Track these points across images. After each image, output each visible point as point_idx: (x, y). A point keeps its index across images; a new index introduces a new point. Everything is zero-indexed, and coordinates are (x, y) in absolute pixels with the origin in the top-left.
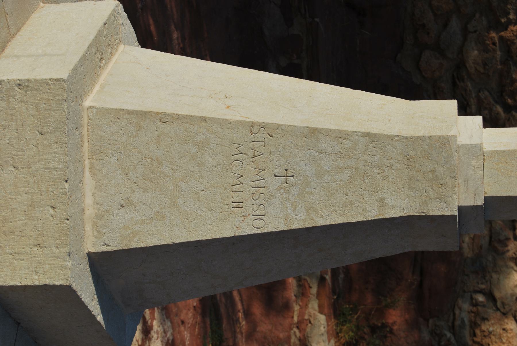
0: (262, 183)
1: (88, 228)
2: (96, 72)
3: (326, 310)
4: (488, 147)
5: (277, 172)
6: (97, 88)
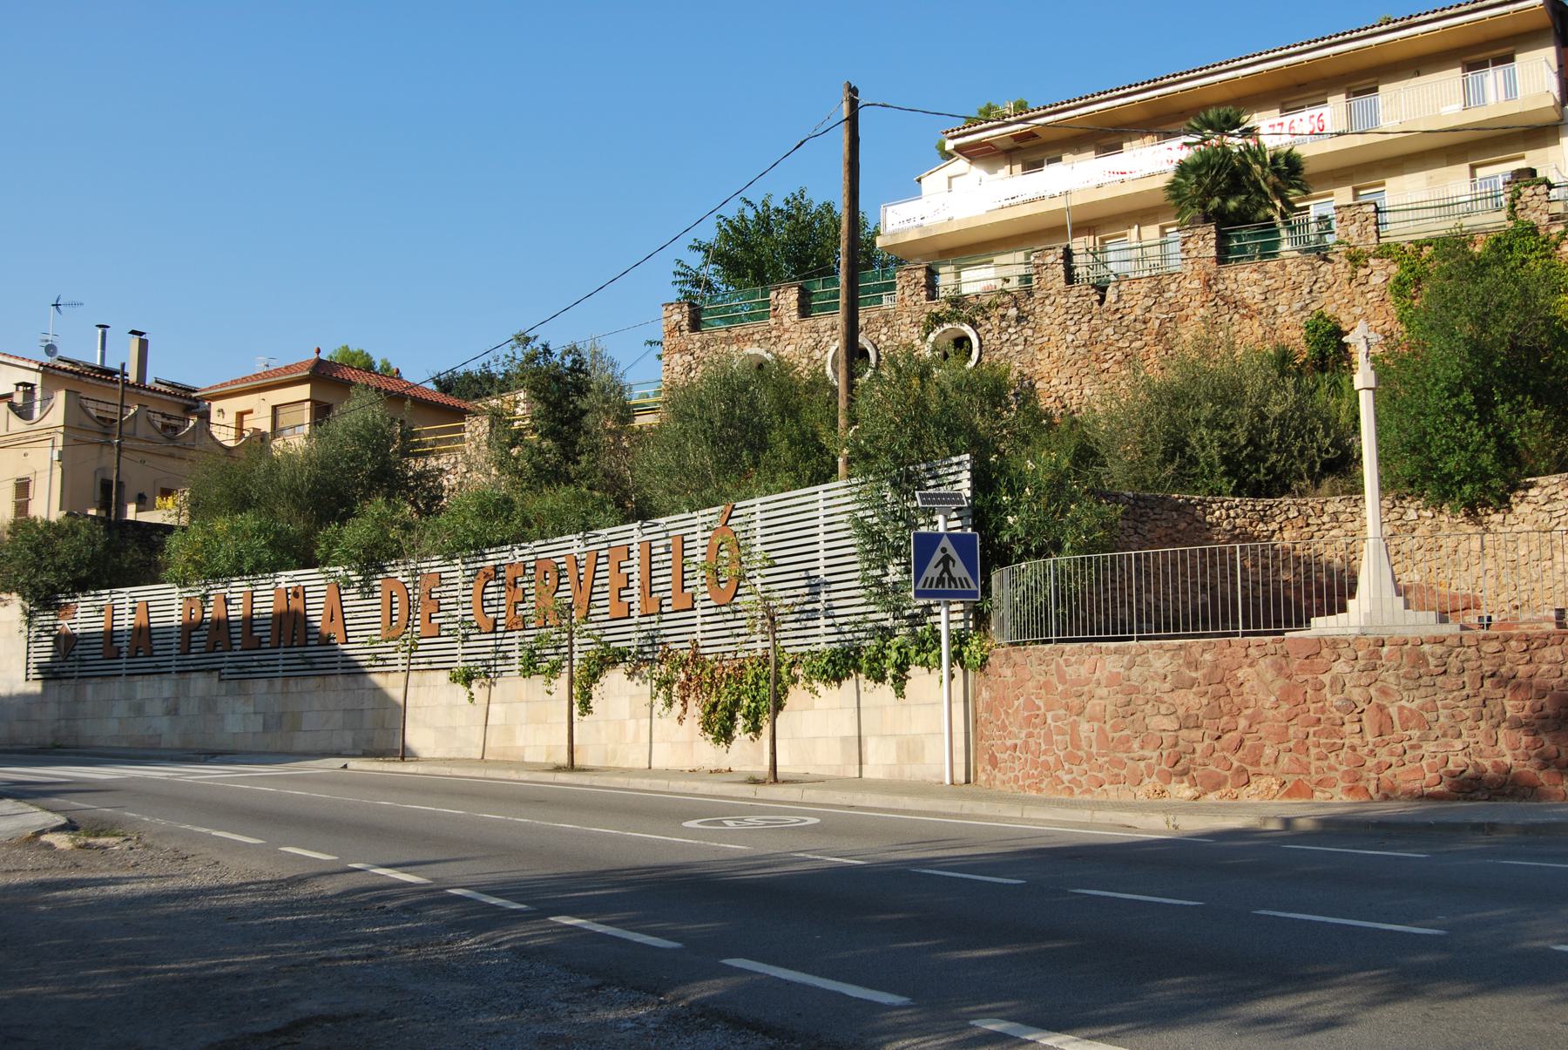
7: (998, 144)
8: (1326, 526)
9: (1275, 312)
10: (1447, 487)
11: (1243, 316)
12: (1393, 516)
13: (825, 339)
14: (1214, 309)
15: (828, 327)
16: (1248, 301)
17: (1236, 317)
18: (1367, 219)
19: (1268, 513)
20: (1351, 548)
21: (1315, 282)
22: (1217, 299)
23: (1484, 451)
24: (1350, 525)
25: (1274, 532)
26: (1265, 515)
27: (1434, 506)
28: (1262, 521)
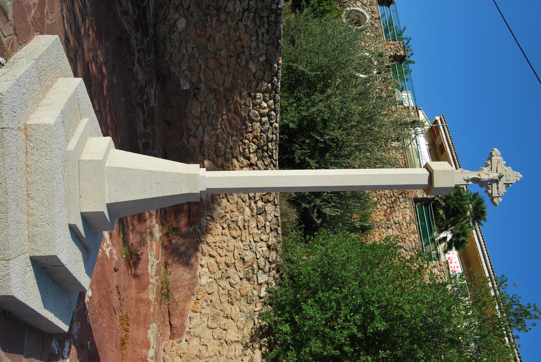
0: (151, 185)
1: (107, 197)
2: (107, 157)
3: (158, 223)
4: (207, 176)
5: (155, 182)
6: (108, 161)
7: (438, 139)
8: (253, 204)
9: (388, 228)
10: (288, 308)
11: (386, 211)
12: (262, 262)
13: (367, 8)
14: (389, 196)
15: (373, 10)
16: (394, 214)
17: (385, 207)
18: (441, 278)
19: (266, 154)
20: (233, 225)
21: (406, 250)
23: (324, 343)
24: (254, 224)
25: (249, 159)
26: (263, 151)
27: (270, 298)
28: (259, 148)
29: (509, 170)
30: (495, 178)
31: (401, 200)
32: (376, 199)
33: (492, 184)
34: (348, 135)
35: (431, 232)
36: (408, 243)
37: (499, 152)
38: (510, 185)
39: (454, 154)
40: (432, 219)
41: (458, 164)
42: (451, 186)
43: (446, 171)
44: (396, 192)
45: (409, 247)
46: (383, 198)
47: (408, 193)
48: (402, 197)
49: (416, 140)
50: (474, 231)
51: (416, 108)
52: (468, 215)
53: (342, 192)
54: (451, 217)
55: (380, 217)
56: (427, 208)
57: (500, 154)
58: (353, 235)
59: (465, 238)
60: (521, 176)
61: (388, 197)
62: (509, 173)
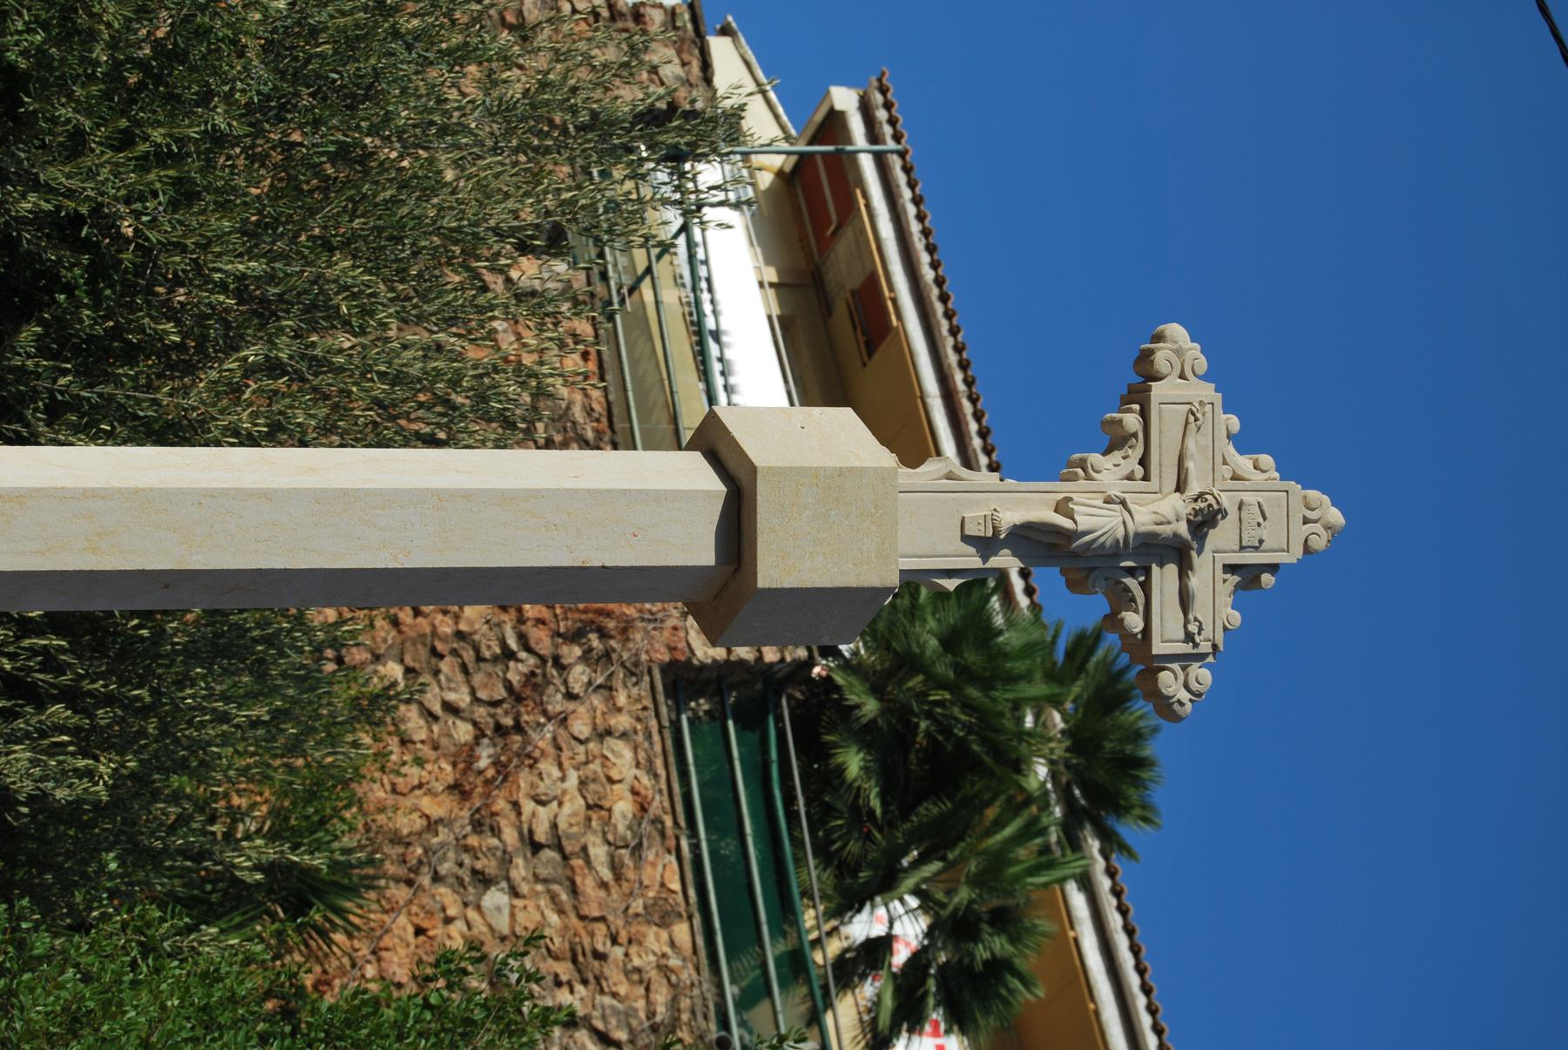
7: (842, 248)
9: (484, 881)
11: (465, 757)
16: (524, 778)
17: (464, 731)
22: (532, 661)
29: (1258, 477)
30: (1166, 530)
31: (579, 676)
32: (394, 670)
33: (1147, 571)
34: (184, 194)
35: (785, 912)
36: (623, 989)
37: (1194, 351)
38: (1267, 579)
39: (952, 358)
40: (792, 816)
41: (973, 426)
42: (875, 582)
43: (842, 473)
44: (540, 622)
45: (630, 1013)
46: (445, 666)
47: (626, 629)
48: (586, 657)
49: (691, 245)
50: (1078, 901)
51: (695, 19)
52: (1032, 784)
53: (134, 614)
54: (919, 800)
55: (426, 804)
56: (754, 737)
57: (1202, 364)
58: (213, 943)
59: (1013, 940)
60: (1336, 516)
61: (480, 659)
62: (1260, 497)
